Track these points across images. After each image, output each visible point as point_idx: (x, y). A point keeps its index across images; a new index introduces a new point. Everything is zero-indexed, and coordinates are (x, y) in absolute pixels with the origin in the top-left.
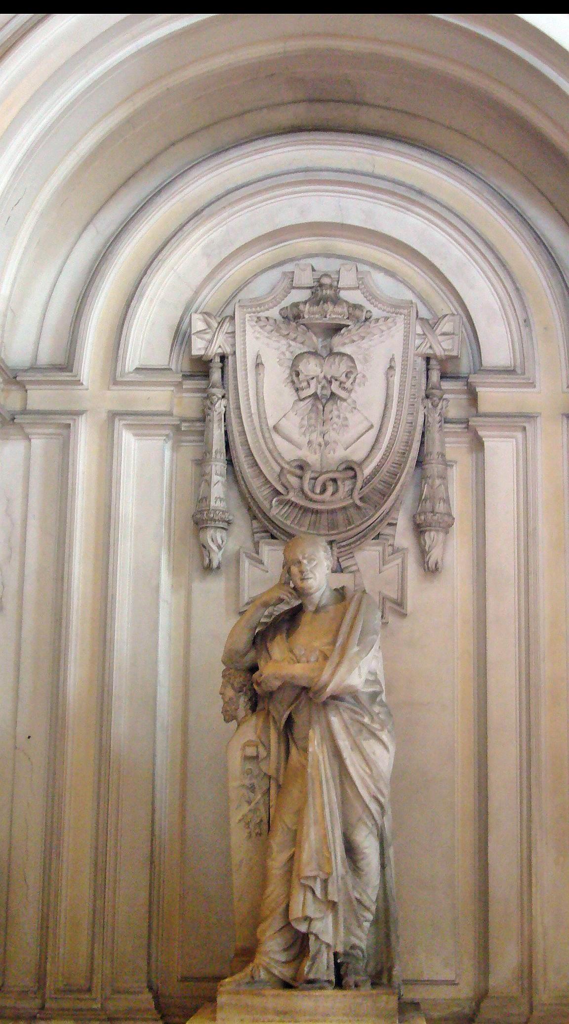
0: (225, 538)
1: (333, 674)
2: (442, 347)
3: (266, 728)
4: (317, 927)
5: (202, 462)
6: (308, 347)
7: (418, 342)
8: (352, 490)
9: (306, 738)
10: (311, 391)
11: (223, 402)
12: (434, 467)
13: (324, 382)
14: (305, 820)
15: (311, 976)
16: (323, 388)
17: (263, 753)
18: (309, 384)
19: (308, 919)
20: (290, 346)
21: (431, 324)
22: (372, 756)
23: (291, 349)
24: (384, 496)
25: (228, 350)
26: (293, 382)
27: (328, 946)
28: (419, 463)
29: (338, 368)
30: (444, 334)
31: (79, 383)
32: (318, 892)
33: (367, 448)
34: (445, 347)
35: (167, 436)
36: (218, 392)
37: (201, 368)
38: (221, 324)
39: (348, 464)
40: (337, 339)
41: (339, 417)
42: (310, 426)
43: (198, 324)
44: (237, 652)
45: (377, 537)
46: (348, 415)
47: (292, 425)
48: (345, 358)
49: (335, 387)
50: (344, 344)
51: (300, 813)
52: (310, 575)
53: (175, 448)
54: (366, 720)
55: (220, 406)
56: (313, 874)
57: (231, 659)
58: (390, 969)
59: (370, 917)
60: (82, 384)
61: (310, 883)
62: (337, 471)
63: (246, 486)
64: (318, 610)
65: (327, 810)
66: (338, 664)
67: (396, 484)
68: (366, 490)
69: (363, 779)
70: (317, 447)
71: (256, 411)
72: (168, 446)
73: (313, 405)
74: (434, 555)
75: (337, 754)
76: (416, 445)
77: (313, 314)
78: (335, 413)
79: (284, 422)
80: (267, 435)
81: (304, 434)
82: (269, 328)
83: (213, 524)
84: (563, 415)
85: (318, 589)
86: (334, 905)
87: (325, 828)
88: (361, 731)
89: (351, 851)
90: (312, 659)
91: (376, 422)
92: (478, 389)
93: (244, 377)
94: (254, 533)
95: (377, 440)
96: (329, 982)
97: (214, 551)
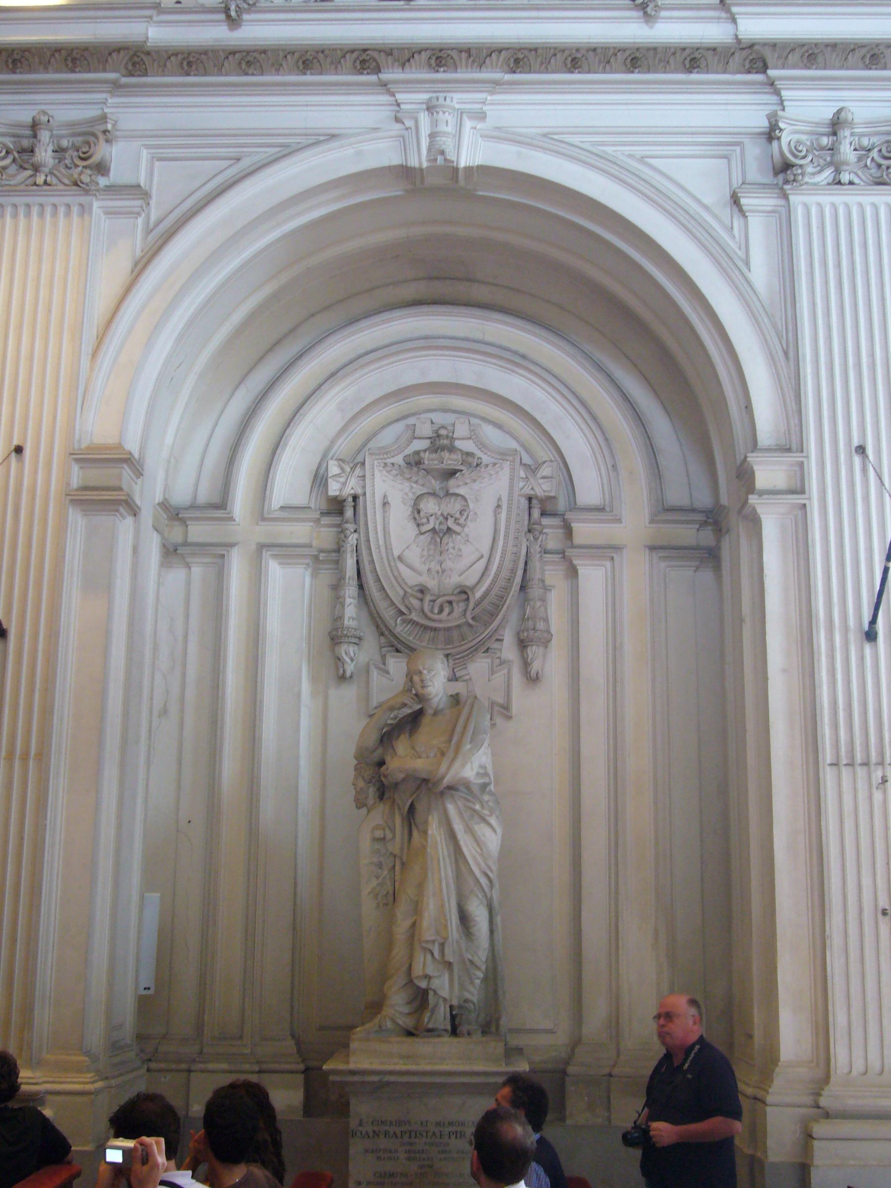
1: (449, 768)
2: (543, 488)
5: (337, 587)
7: (521, 484)
8: (465, 611)
9: (426, 822)
10: (430, 526)
11: (355, 536)
12: (535, 592)
13: (441, 518)
15: (430, 1026)
16: (440, 523)
17: (389, 835)
19: (428, 977)
20: (412, 487)
21: (532, 469)
22: (483, 838)
23: (414, 490)
25: (359, 491)
26: (415, 519)
27: (445, 1000)
28: (523, 588)
29: (453, 506)
30: (543, 478)
31: (232, 519)
34: (545, 489)
35: (307, 564)
36: (351, 527)
38: (353, 469)
40: (452, 482)
41: (454, 548)
42: (429, 556)
43: (334, 469)
46: (462, 547)
47: (414, 556)
49: (450, 523)
50: (459, 486)
52: (430, 684)
53: (314, 575)
54: (478, 807)
55: (352, 539)
56: (432, 938)
57: (361, 755)
58: (498, 1020)
59: (481, 975)
61: (429, 946)
62: (453, 594)
65: (444, 884)
66: (453, 760)
67: (503, 605)
69: (474, 858)
73: (432, 538)
74: (535, 667)
75: (452, 836)
76: (520, 572)
77: (432, 460)
78: (451, 545)
79: (406, 553)
80: (392, 564)
81: (424, 563)
82: (394, 472)
86: (449, 965)
88: (472, 816)
89: (464, 918)
92: (572, 525)
94: (381, 648)
95: (486, 568)
96: (446, 1030)
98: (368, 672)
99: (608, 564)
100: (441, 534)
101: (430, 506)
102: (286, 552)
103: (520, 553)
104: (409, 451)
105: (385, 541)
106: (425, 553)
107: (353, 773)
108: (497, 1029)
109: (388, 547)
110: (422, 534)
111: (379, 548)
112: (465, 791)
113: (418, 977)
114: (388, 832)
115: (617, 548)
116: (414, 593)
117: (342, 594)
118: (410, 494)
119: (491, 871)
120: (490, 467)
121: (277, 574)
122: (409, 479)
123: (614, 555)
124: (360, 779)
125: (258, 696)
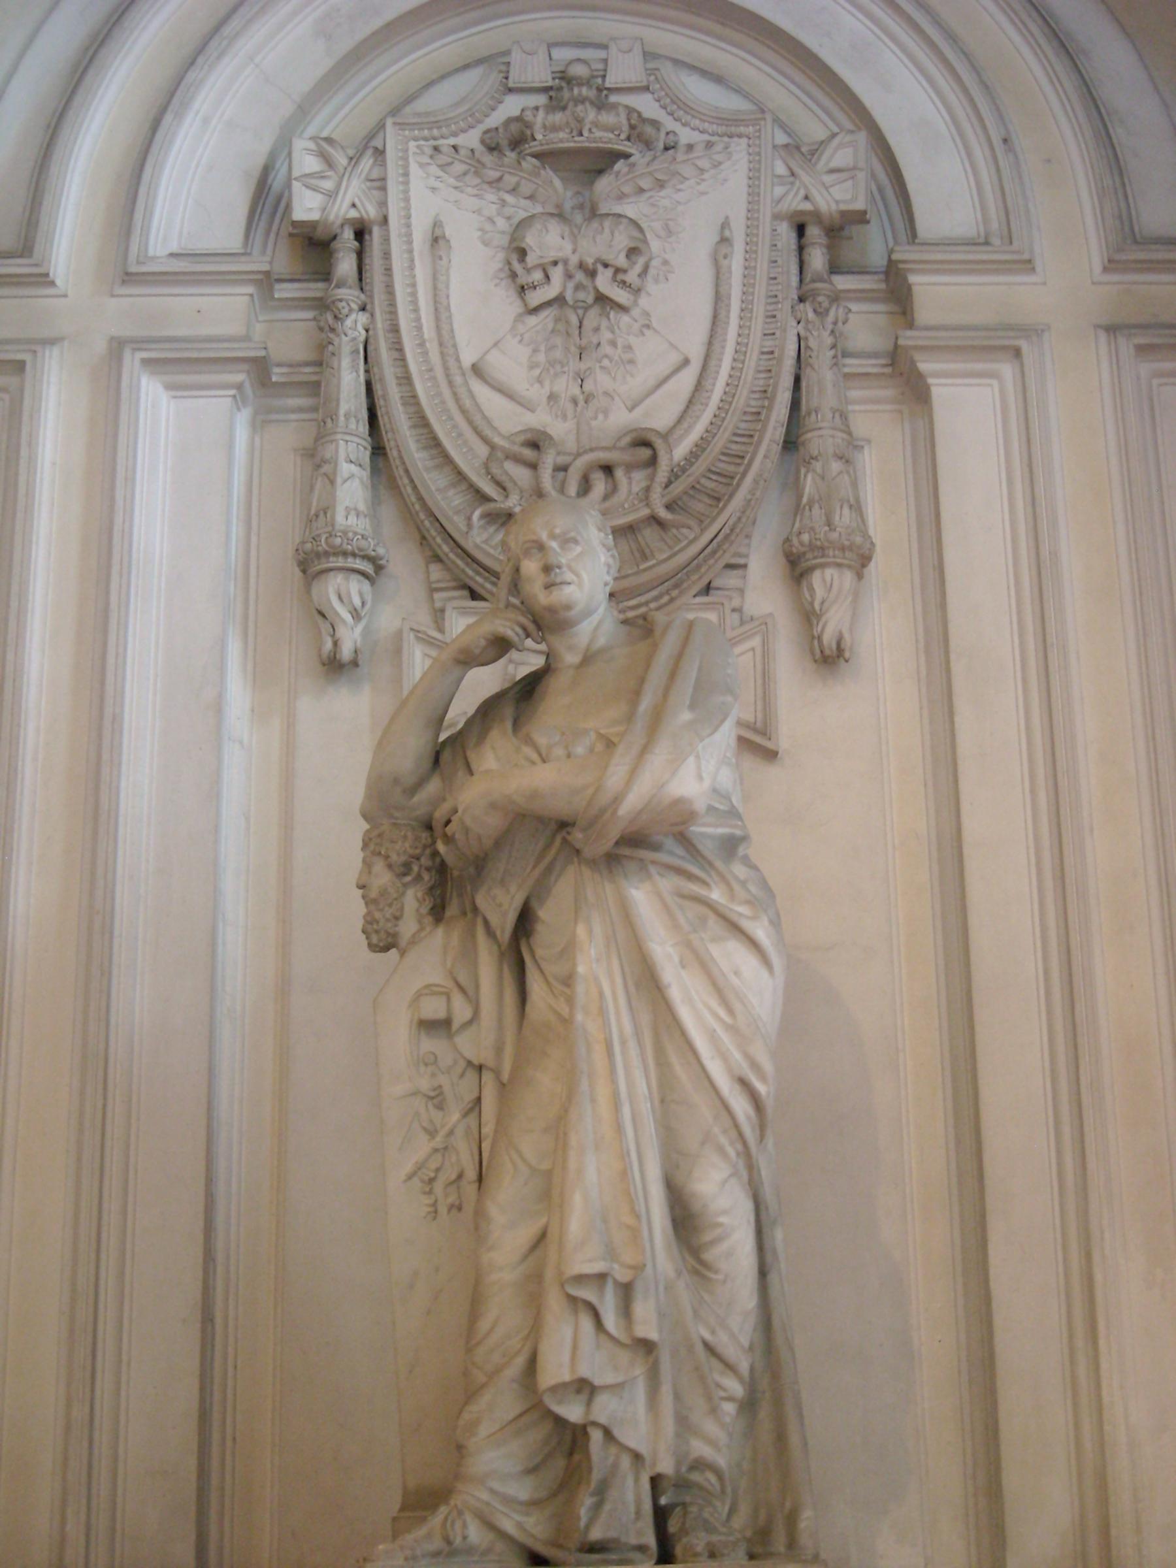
0: (369, 598)
1: (633, 773)
2: (834, 195)
3: (469, 952)
4: (605, 1409)
5: (316, 458)
6: (543, 204)
7: (779, 191)
8: (648, 489)
9: (569, 950)
10: (551, 292)
11: (363, 318)
12: (821, 438)
13: (580, 276)
14: (573, 1140)
15: (596, 1534)
16: (579, 287)
17: (461, 1011)
18: (547, 277)
19: (585, 1388)
20: (503, 203)
21: (802, 153)
22: (735, 980)
23: (508, 211)
24: (718, 500)
25: (371, 211)
26: (514, 275)
27: (637, 1457)
28: (791, 444)
29: (610, 243)
30: (832, 171)
31: (44, 280)
32: (610, 1320)
33: (677, 408)
34: (838, 197)
35: (239, 387)
36: (349, 295)
37: (315, 246)
38: (354, 160)
39: (634, 435)
40: (604, 184)
41: (613, 344)
42: (552, 363)
43: (307, 162)
44: (396, 781)
45: (707, 589)
46: (632, 340)
47: (513, 364)
48: (624, 221)
49: (603, 280)
50: (622, 197)
51: (559, 1129)
52: (569, 576)
53: (259, 423)
54: (716, 895)
55: (355, 325)
56: (598, 1267)
57: (383, 805)
58: (792, 1520)
59: (736, 1388)
60: (52, 284)
61: (587, 1293)
62: (614, 447)
63: (415, 488)
64: (588, 659)
65: (626, 1111)
66: (645, 750)
67: (744, 474)
68: (678, 487)
69: (713, 1037)
70: (569, 407)
71: (433, 334)
72: (242, 420)
73: (557, 320)
74: (834, 623)
75: (647, 982)
76: (784, 397)
77: (555, 129)
78: (606, 335)
79: (494, 358)
80: (458, 380)
81: (539, 380)
82: (459, 168)
83: (340, 562)
84: (1097, 326)
85: (587, 613)
86: (647, 1347)
87: (624, 1155)
88: (703, 920)
89: (686, 1220)
90: (580, 750)
91: (696, 351)
92: (913, 279)
93: (404, 258)
94: (432, 590)
95: (699, 386)
96: (642, 1548)
97: (344, 622)
98: (398, 651)
99: (1007, 370)
100: (583, 304)
101: (549, 241)
102: (182, 363)
103: (782, 349)
104: (496, 119)
105: (438, 328)
106: (541, 357)
107: (360, 865)
108: (792, 1543)
109: (447, 344)
110: (535, 310)
111: (422, 344)
112: (680, 851)
113: (559, 1389)
114: (458, 1001)
115: (1034, 332)
116: (516, 449)
117: (328, 453)
118: (501, 223)
119: (763, 1078)
120: (699, 151)
121: (159, 411)
122: (496, 183)
123: (1024, 345)
124: (379, 866)
125: (108, 711)
